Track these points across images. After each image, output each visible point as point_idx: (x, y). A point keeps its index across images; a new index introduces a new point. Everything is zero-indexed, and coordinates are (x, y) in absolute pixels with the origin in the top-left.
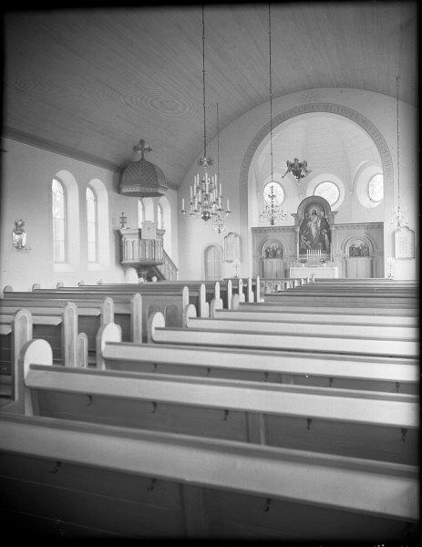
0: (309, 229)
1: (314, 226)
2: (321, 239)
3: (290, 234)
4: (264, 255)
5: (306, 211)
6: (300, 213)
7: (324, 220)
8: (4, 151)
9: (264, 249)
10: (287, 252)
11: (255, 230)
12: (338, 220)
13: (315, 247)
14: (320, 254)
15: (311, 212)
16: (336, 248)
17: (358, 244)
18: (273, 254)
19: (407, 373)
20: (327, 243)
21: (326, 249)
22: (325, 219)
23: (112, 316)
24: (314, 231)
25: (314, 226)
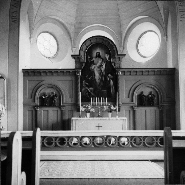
0: (92, 73)
1: (97, 70)
2: (105, 83)
3: (69, 78)
4: (37, 102)
5: (89, 53)
6: (82, 54)
7: (109, 65)
8: (155, 80)
9: (38, 95)
10: (67, 99)
11: (27, 72)
12: (125, 64)
13: (99, 95)
14: (105, 104)
15: (94, 54)
16: (123, 95)
17: (147, 92)
18: (48, 101)
19: (184, 10)
20: (112, 90)
21: (113, 99)
22: (110, 63)
23: (40, 136)
24: (97, 75)
25: (97, 70)
